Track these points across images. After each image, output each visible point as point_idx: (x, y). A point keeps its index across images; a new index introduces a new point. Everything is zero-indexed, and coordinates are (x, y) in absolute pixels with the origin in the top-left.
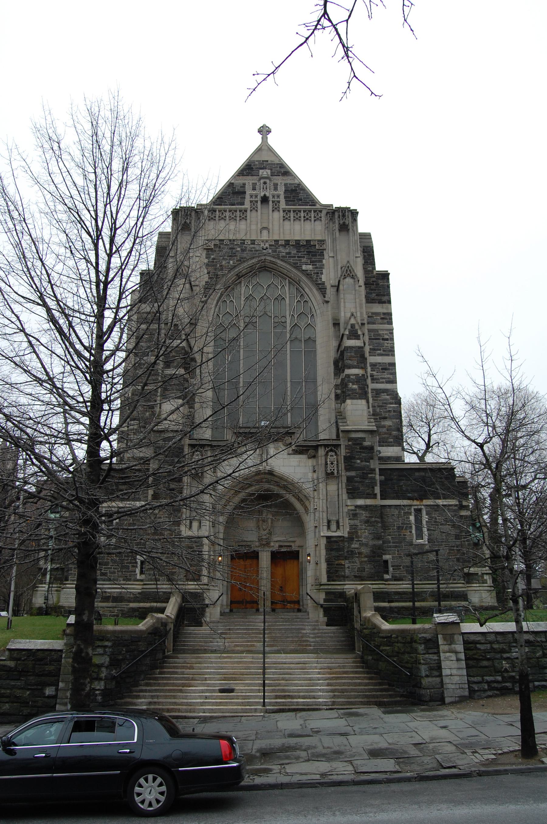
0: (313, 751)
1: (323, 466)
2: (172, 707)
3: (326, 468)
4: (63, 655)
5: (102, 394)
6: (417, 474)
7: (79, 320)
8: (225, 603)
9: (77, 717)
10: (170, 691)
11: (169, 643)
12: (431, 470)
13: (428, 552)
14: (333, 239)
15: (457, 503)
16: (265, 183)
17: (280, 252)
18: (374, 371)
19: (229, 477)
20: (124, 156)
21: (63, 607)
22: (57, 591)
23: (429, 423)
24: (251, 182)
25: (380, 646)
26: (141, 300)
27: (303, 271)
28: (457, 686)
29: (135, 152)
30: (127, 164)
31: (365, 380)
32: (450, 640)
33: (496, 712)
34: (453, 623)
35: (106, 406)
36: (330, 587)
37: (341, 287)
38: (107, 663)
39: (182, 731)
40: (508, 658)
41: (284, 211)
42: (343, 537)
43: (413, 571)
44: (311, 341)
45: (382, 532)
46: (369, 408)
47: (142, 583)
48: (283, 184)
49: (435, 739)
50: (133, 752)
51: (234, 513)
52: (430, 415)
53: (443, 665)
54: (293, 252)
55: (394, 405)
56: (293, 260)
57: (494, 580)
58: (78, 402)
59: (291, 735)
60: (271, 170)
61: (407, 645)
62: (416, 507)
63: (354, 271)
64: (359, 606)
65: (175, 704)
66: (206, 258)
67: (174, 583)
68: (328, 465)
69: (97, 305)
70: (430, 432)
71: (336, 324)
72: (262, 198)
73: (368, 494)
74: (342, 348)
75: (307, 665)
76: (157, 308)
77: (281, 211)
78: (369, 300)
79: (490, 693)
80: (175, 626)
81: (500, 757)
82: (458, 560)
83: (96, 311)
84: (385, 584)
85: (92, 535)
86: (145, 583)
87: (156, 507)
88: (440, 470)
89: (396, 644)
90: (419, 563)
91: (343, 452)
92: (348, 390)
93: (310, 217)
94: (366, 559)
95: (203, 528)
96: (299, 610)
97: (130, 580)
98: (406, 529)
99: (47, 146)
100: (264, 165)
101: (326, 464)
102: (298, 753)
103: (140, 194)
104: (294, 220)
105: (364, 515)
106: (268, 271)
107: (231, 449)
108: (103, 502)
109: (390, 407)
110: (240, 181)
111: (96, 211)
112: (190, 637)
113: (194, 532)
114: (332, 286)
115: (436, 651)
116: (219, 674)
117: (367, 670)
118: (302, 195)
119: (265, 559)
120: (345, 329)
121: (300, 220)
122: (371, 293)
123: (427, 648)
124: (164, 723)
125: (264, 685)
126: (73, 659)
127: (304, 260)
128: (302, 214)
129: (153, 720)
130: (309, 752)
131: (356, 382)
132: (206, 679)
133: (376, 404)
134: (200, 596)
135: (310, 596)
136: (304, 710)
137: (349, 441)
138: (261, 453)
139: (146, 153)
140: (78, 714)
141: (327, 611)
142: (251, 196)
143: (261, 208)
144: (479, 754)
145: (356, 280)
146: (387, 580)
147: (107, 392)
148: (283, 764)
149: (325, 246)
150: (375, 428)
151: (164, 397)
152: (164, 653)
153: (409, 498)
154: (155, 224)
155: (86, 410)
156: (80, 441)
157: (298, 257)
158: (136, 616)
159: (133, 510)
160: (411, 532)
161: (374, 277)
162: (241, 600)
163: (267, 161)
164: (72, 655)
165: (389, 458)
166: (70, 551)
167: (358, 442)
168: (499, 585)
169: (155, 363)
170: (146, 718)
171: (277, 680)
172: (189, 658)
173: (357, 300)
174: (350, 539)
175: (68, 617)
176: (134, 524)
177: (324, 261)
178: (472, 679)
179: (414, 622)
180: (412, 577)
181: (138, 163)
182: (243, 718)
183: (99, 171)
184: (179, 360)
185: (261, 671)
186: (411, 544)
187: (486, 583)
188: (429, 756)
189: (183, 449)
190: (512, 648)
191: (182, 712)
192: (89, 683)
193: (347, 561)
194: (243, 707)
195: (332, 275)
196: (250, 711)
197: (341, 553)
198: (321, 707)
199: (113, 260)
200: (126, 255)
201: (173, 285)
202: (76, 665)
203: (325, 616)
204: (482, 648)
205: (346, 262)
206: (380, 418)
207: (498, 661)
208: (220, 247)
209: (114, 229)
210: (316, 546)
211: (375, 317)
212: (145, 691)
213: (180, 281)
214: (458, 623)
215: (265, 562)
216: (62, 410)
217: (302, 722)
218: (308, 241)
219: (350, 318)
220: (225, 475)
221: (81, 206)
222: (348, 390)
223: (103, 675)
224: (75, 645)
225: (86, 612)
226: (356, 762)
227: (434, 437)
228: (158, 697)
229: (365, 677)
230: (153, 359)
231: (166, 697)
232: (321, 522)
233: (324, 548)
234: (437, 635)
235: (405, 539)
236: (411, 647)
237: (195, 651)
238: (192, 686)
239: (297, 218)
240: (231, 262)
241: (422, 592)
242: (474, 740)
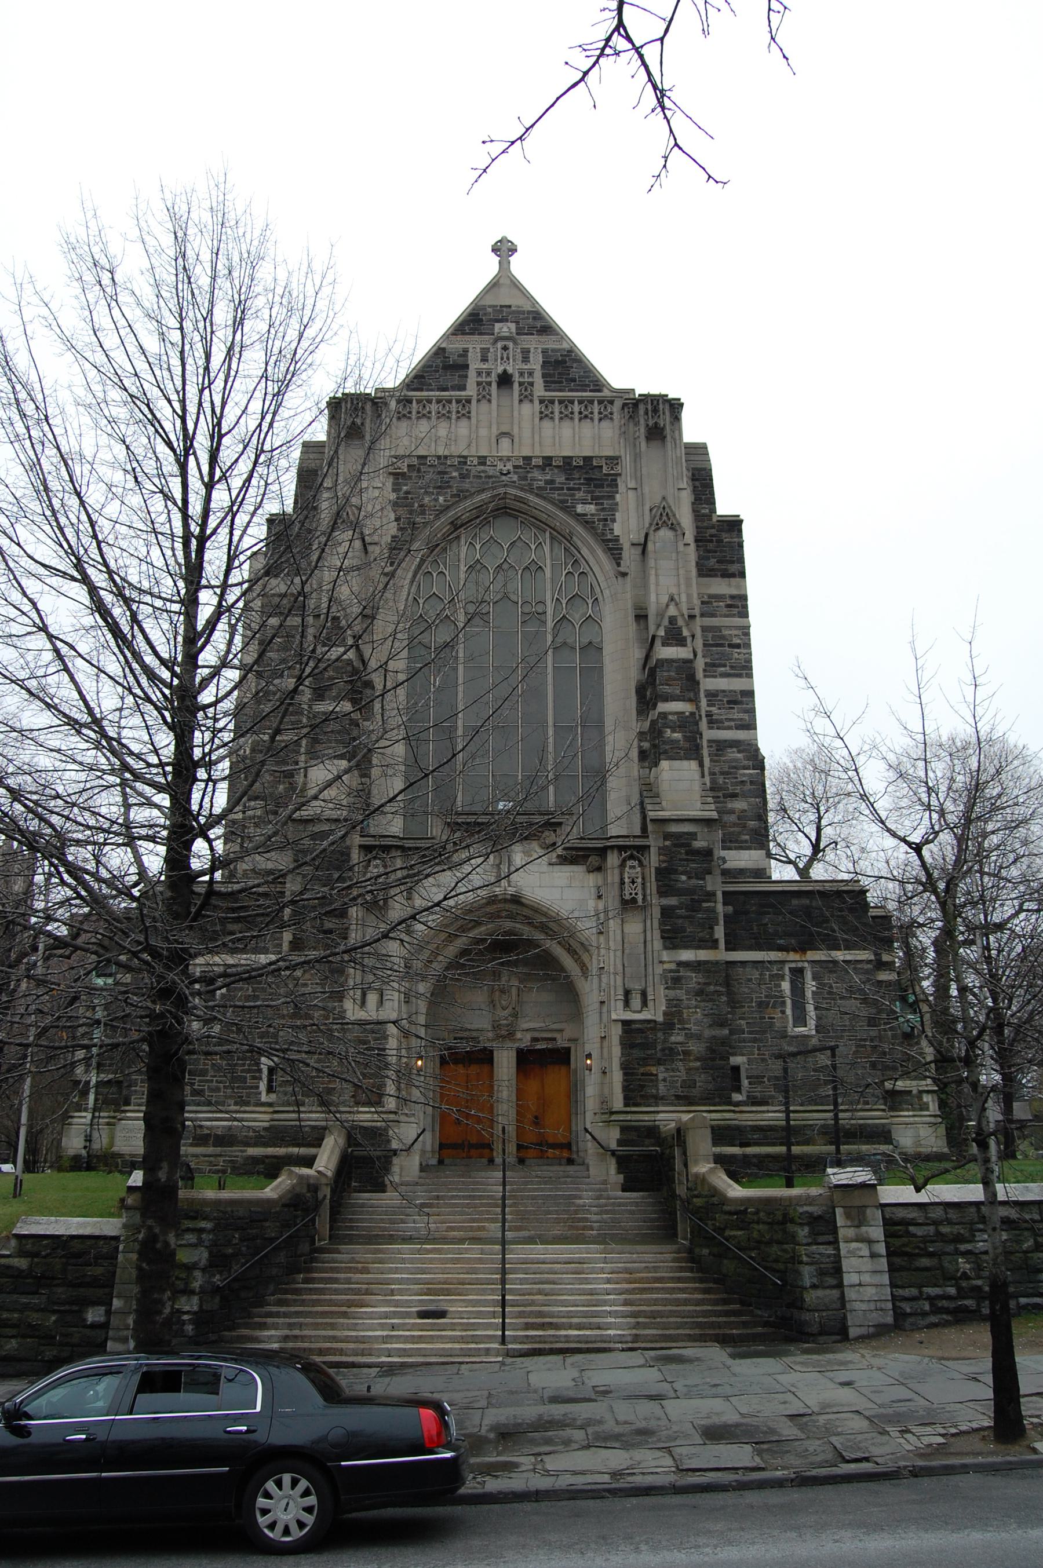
0: (597, 1428)
1: (617, 886)
2: (328, 1345)
3: (622, 890)
4: (121, 1247)
5: (195, 749)
6: (795, 902)
7: (150, 610)
8: (429, 1148)
9: (147, 1365)
10: (324, 1314)
11: (323, 1223)
12: (822, 894)
13: (815, 1050)
14: (636, 455)
15: (872, 957)
16: (505, 348)
17: (533, 479)
18: (713, 705)
19: (437, 909)
20: (236, 296)
21: (120, 1155)
22: (108, 1124)
23: (818, 804)
24: (478, 347)
25: (724, 1229)
26: (269, 572)
27: (579, 515)
28: (872, 1306)
29: (258, 289)
30: (243, 312)
31: (697, 724)
32: (858, 1217)
33: (946, 1355)
34: (863, 1186)
35: (201, 774)
36: (629, 1117)
37: (650, 546)
38: (204, 1262)
39: (347, 1391)
40: (969, 1253)
41: (541, 402)
42: (655, 1021)
43: (787, 1086)
44: (593, 649)
45: (729, 1013)
46: (703, 776)
47: (271, 1110)
48: (540, 350)
49: (829, 1406)
50: (254, 1431)
51: (445, 977)
52: (819, 790)
53: (845, 1265)
54: (558, 480)
55: (751, 771)
56: (559, 495)
57: (942, 1104)
58: (149, 765)
59: (555, 1400)
60: (517, 323)
61: (776, 1227)
62: (793, 965)
63: (674, 515)
64: (685, 1153)
65: (334, 1339)
66: (394, 490)
67: (332, 1109)
68: (626, 885)
69: (185, 580)
70: (820, 821)
71: (641, 617)
72: (499, 376)
73: (701, 940)
74: (653, 662)
75: (585, 1266)
76: (300, 586)
77: (536, 402)
78: (704, 571)
79: (934, 1319)
80: (333, 1191)
81: (952, 1440)
82: (873, 1065)
83: (183, 592)
84: (734, 1112)
85: (175, 1017)
86: (277, 1109)
87: (297, 964)
88: (839, 894)
89: (756, 1226)
90: (798, 1071)
91: (654, 859)
92: (664, 743)
93: (592, 413)
94: (699, 1064)
95: (387, 1005)
96: (570, 1162)
97: (247, 1104)
98: (774, 1007)
99: (89, 278)
100: (503, 314)
101: (622, 883)
102: (568, 1432)
103: (266, 370)
104: (561, 418)
105: (694, 980)
106: (510, 515)
107: (440, 855)
108: (196, 956)
109: (744, 775)
110: (459, 344)
111: (183, 402)
112: (361, 1213)
113: (370, 1012)
114: (633, 545)
115: (831, 1238)
116: (417, 1282)
117: (700, 1275)
118: (575, 372)
119: (505, 1064)
120: (658, 626)
121: (572, 419)
122: (708, 558)
123: (813, 1233)
124: (312, 1375)
125: (503, 1303)
126: (140, 1253)
127: (579, 495)
128: (576, 408)
129: (291, 1371)
130: (590, 1430)
131: (680, 727)
132: (392, 1292)
133: (717, 770)
134: (381, 1135)
135: (590, 1134)
136: (579, 1351)
137: (665, 839)
138: (497, 862)
139: (279, 291)
140: (148, 1359)
141: (623, 1163)
142: (479, 374)
143: (498, 396)
144: (914, 1434)
145: (679, 532)
146: (738, 1104)
147: (203, 746)
148: (539, 1454)
149: (619, 468)
150: (714, 815)
151: (313, 755)
152: (313, 1242)
153: (781, 949)
154: (296, 426)
155: (163, 781)
156: (152, 839)
157: (569, 489)
158: (258, 1173)
159: (254, 970)
160: (783, 1012)
161: (713, 527)
162: (460, 1142)
163: (510, 306)
164: (137, 1246)
165: (742, 872)
166: (134, 1049)
167: (682, 841)
168: (951, 1113)
169: (295, 690)
170: (278, 1367)
171: (529, 1294)
172: (361, 1252)
173: (682, 572)
174: (668, 1026)
175: (130, 1174)
176: (255, 998)
177: (618, 497)
178: (900, 1292)
179: (790, 1184)
180: (786, 1098)
181: (263, 310)
182: (463, 1366)
183: (188, 325)
184: (341, 685)
185: (498, 1276)
186: (784, 1035)
187: (927, 1109)
188: (819, 1439)
189: (348, 855)
190: (977, 1234)
191: (346, 1355)
192: (169, 1299)
193: (662, 1068)
194: (464, 1346)
195: (633, 523)
196: (477, 1352)
197: (649, 1052)
198: (612, 1345)
199: (215, 494)
200: (240, 484)
201: (330, 543)
202: (144, 1265)
203: (619, 1171)
204: (920, 1233)
205: (660, 499)
206: (725, 796)
207: (949, 1258)
208: (419, 470)
209: (217, 436)
210: (603, 1038)
211: (715, 604)
212: (277, 1315)
213: (344, 536)
214: (874, 1186)
215: (505, 1070)
216: (118, 781)
217: (576, 1374)
218: (587, 459)
219: (667, 606)
220: (430, 904)
221: (154, 393)
222: (664, 743)
223: (196, 1285)
224: (142, 1227)
225: (165, 1165)
226: (678, 1450)
227: (828, 832)
228: (301, 1326)
229: (696, 1289)
230: (291, 683)
231: (316, 1326)
232: (612, 992)
233: (618, 1042)
234: (834, 1208)
235: (772, 1025)
236: (785, 1231)
237: (372, 1239)
238: (367, 1306)
239: (566, 416)
240: (441, 499)
241: (805, 1126)
242: (904, 1409)
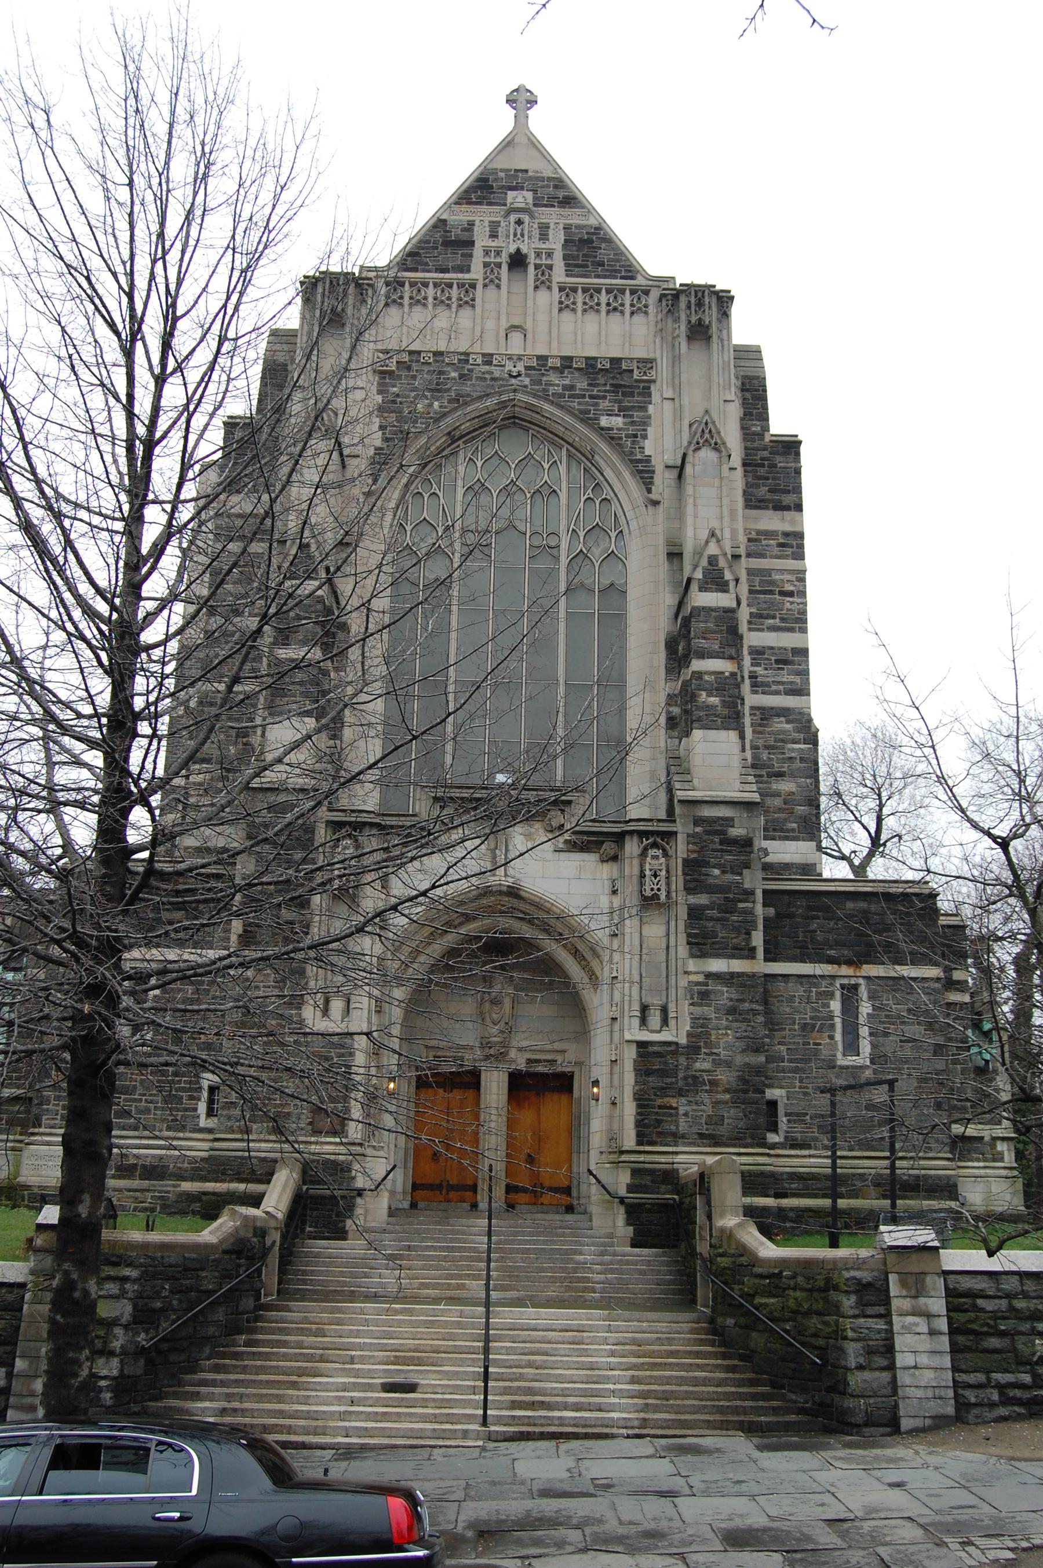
0: (596, 1529)
1: (635, 879)
2: (274, 1421)
3: (642, 884)
4: (28, 1296)
5: (136, 698)
6: (850, 905)
7: (86, 528)
8: (399, 1188)
9: (61, 1436)
10: (269, 1384)
11: (270, 1275)
12: (888, 897)
13: (869, 1083)
14: (674, 357)
15: (942, 975)
16: (519, 222)
17: (549, 384)
18: (758, 665)
19: (421, 899)
20: (199, 148)
21: (28, 1187)
22: (13, 1149)
23: (879, 789)
24: (487, 219)
25: (753, 1296)
26: (231, 486)
27: (602, 429)
28: (930, 1394)
29: (225, 139)
30: (206, 167)
31: (738, 686)
32: (916, 1286)
33: (1018, 1454)
34: (923, 1249)
35: (144, 728)
36: (642, 1158)
37: (688, 469)
38: (126, 1318)
39: (300, 1474)
41: (561, 289)
42: (677, 1044)
43: (833, 1125)
44: (616, 592)
45: (767, 1036)
46: (743, 750)
47: (211, 1137)
48: (561, 226)
49: (877, 1511)
50: (189, 1518)
51: (431, 981)
52: (883, 770)
53: (899, 1342)
54: (579, 386)
55: (802, 746)
56: (579, 404)
57: (1019, 1155)
58: (79, 716)
59: (546, 1493)
60: (535, 191)
61: (816, 1295)
62: (845, 981)
63: (719, 433)
64: (708, 1203)
65: (282, 1414)
66: (379, 392)
67: (291, 1138)
68: (647, 879)
69: (129, 492)
70: (881, 810)
71: (675, 555)
72: (511, 256)
73: (735, 948)
74: (687, 611)
75: (585, 1334)
76: (268, 505)
77: (555, 289)
78: (752, 502)
79: (1003, 1411)
80: (284, 1237)
81: (1024, 1555)
82: (938, 1106)
83: (126, 508)
84: (768, 1155)
85: (105, 1020)
86: (218, 1136)
87: (253, 961)
88: (905, 896)
89: (791, 1293)
90: (849, 1106)
91: (681, 848)
92: (698, 708)
93: (622, 305)
94: (728, 1096)
95: (355, 1014)
96: (570, 1209)
97: (183, 1128)
98: (820, 1031)
99: (19, 118)
100: (517, 180)
101: (642, 876)
102: (562, 1532)
103: (233, 237)
104: (585, 311)
105: (725, 995)
106: (522, 428)
107: (430, 834)
108: (129, 948)
109: (793, 750)
110: (461, 216)
111: (131, 274)
112: (316, 1264)
114: (667, 467)
115: (881, 1310)
116: (383, 1348)
117: (723, 1349)
118: (604, 254)
119: (494, 1090)
120: (695, 566)
121: (598, 311)
122: (758, 486)
123: (862, 1304)
124: (259, 1453)
125: (486, 1377)
126: (53, 1303)
127: (604, 404)
128: (604, 298)
129: (234, 1447)
130: (588, 1530)
131: (717, 689)
132: (352, 1360)
133: (760, 743)
134: (342, 1170)
135: (595, 1176)
136: (576, 1436)
137: (696, 824)
139: (252, 143)
140: (59, 1429)
141: (633, 1213)
142: (487, 253)
144: (977, 1547)
145: (724, 453)
146: (773, 1146)
147: (149, 692)
148: (527, 1557)
149: (653, 373)
150: (756, 797)
151: (272, 709)
152: (258, 1298)
153: (831, 961)
154: (269, 308)
155: (99, 736)
156: (81, 805)
157: (591, 397)
158: (194, 1213)
159: (200, 966)
160: (831, 1037)
161: (765, 449)
162: (437, 1182)
163: (526, 171)
164: (49, 1296)
165: (787, 866)
166: (52, 1058)
167: (716, 828)
168: (1029, 1167)
169: (259, 631)
170: (218, 1443)
171: (517, 1367)
172: (314, 1311)
173: (725, 501)
174: (693, 1049)
175: (40, 1209)
176: (198, 1001)
177: (651, 408)
178: (963, 1377)
179: (834, 1244)
180: (834, 1138)
181: (231, 166)
182: (436, 1451)
183: (139, 181)
184: (308, 626)
185: (481, 1344)
187: (1002, 1160)
188: (863, 1549)
189: (313, 832)
191: (295, 1434)
192: (87, 1359)
193: (683, 1100)
194: (437, 1426)
195: (668, 441)
196: (453, 1434)
197: (669, 1080)
198: (615, 1431)
199: (167, 389)
200: (198, 379)
201: (308, 452)
202: (58, 1317)
203: (628, 1223)
204: (989, 1308)
205: (702, 412)
206: (769, 775)
207: (1023, 1338)
208: (409, 368)
209: (171, 319)
211: (764, 542)
212: (213, 1383)
213: (321, 445)
214: (936, 1249)
215: (494, 1097)
216: (41, 734)
217: (571, 1463)
218: (616, 361)
219: (707, 542)
220: (415, 893)
221: (95, 263)
222: (698, 708)
223: (117, 1345)
224: (58, 1271)
225: (87, 1197)
226: (693, 1557)
227: (890, 823)
228: (241, 1397)
229: (717, 1366)
230: (253, 623)
231: (261, 1398)
232: (626, 1008)
234: (887, 1274)
235: (817, 1053)
236: (826, 1300)
237: (328, 1296)
238: (321, 1376)
239: (591, 307)
240: (436, 404)
241: (854, 1175)
242: (966, 1517)
